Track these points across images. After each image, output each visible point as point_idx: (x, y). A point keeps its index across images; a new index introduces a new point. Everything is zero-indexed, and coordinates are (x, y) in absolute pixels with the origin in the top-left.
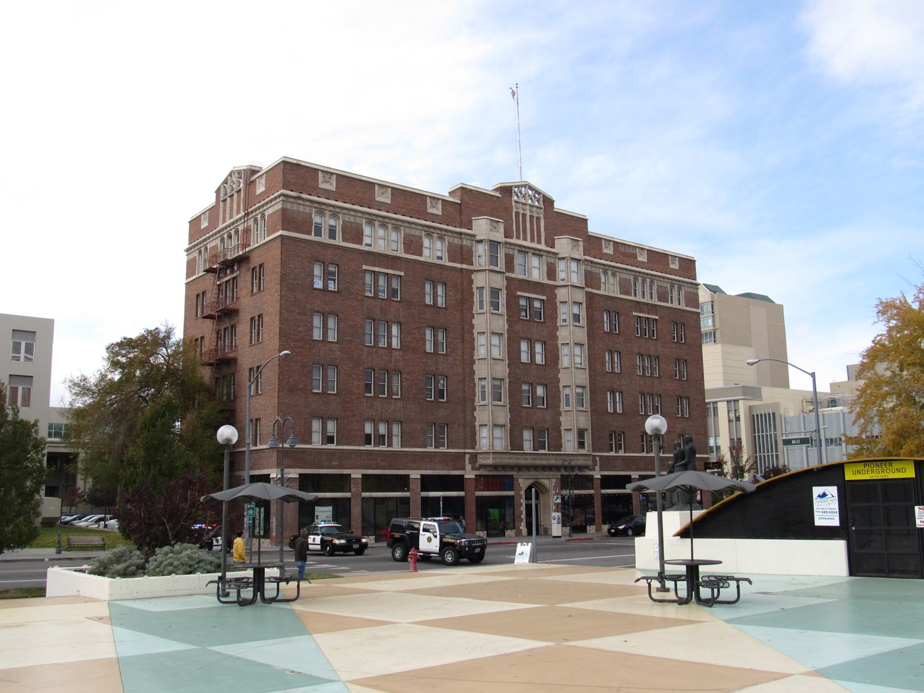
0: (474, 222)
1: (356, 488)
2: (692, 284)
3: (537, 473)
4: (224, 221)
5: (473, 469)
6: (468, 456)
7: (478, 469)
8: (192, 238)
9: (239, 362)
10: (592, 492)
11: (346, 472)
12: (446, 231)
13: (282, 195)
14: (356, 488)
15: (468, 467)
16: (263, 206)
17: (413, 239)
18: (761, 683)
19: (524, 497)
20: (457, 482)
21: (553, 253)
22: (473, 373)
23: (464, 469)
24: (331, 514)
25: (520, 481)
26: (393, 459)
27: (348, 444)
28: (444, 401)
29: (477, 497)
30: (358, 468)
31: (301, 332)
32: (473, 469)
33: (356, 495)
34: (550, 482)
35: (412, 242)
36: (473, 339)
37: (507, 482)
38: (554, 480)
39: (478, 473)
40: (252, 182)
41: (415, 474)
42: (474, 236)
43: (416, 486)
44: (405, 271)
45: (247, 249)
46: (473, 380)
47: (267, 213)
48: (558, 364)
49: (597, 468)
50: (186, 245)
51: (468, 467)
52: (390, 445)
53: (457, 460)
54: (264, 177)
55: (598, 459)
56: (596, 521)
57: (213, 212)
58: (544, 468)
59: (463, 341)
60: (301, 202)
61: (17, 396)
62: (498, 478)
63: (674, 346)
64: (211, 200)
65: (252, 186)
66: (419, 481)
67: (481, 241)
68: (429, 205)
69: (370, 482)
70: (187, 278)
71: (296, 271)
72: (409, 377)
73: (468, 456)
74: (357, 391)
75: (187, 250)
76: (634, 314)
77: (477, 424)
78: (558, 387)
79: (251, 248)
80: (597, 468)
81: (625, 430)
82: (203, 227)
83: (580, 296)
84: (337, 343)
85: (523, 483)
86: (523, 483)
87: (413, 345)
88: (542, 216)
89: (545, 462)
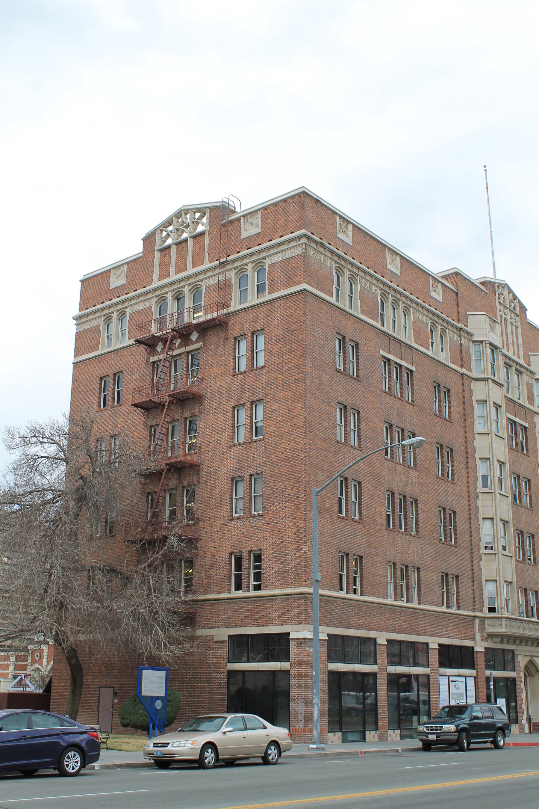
3: (533, 649)
4: (164, 274)
6: (477, 621)
8: (84, 303)
9: (206, 468)
10: (392, 669)
11: (371, 634)
13: (305, 235)
15: (478, 636)
16: (123, 302)
29: (389, 674)
30: (383, 630)
40: (231, 222)
45: (225, 311)
47: (267, 263)
50: (75, 311)
54: (260, 213)
57: (136, 268)
59: (467, 466)
60: (321, 250)
61: (358, 419)
64: (136, 248)
65: (231, 228)
70: (76, 356)
75: (76, 319)
79: (231, 309)
82: (112, 286)
87: (426, 465)
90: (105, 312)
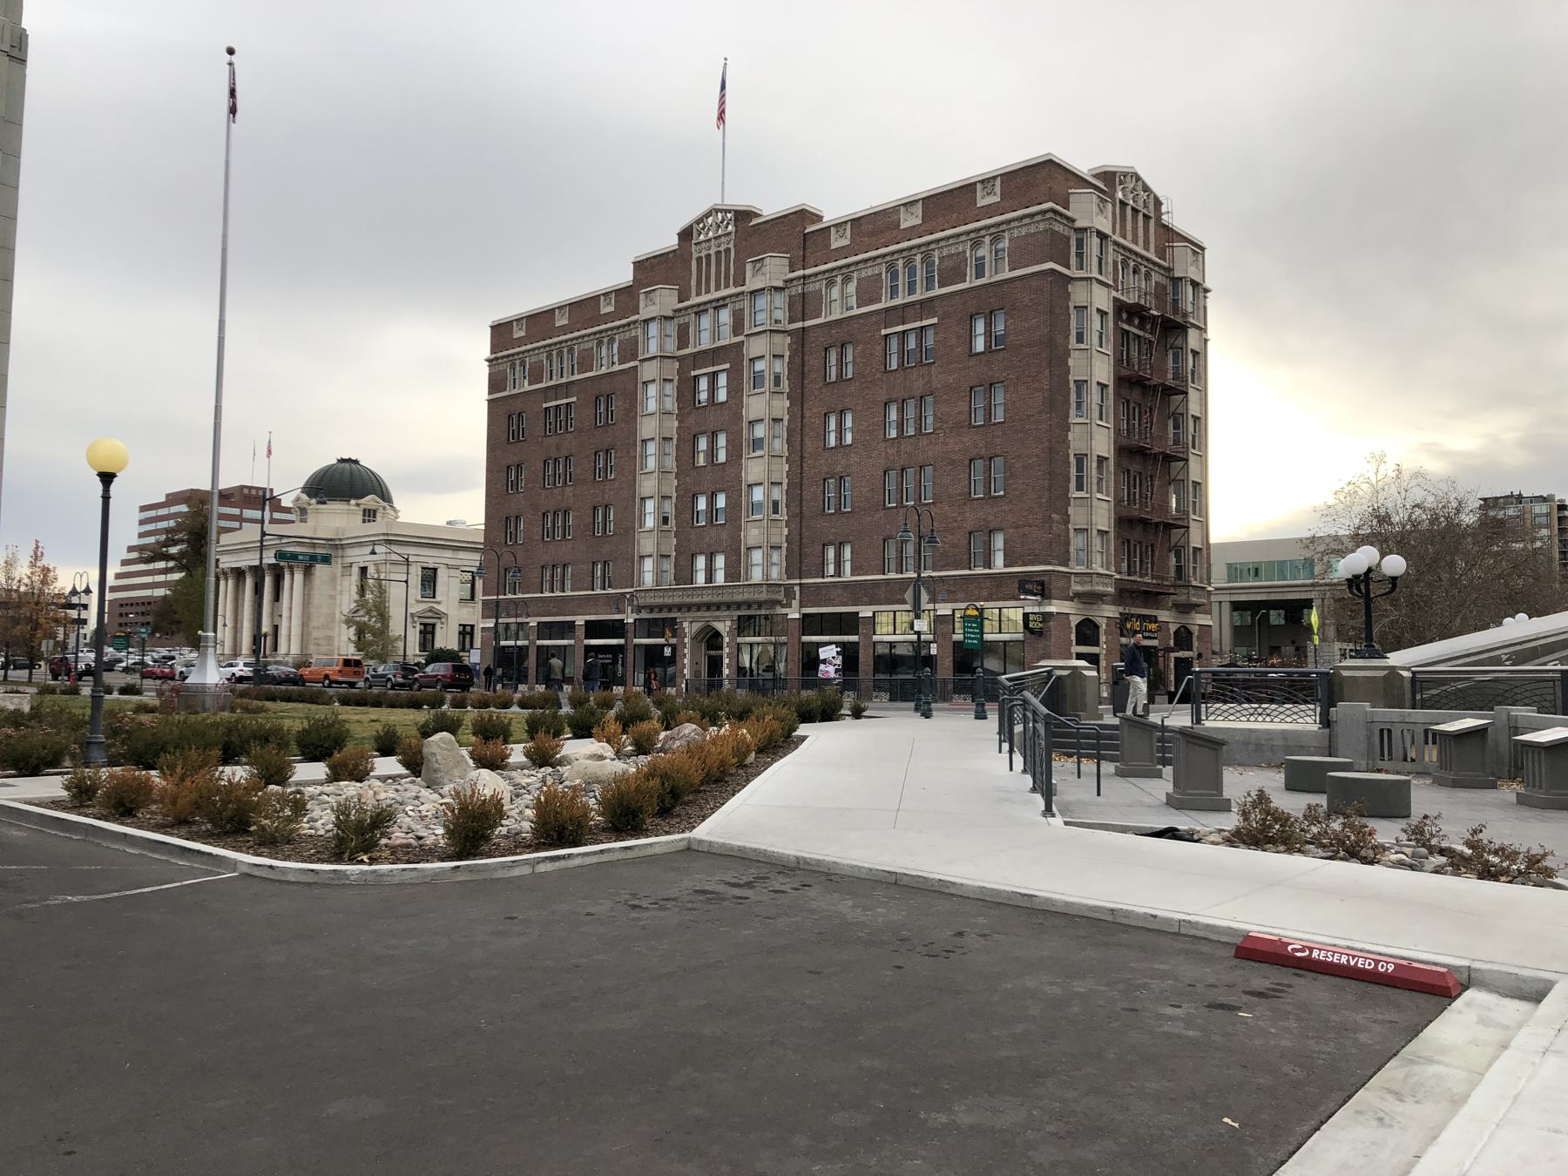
12: (848, 266)
18: (1491, 991)
19: (1102, 631)
20: (616, 629)
21: (1067, 218)
25: (685, 625)
37: (671, 625)
38: (728, 623)
42: (1073, 221)
43: (581, 633)
49: (795, 603)
52: (988, 565)
53: (617, 602)
55: (797, 589)
58: (718, 606)
80: (795, 603)
83: (783, 344)
85: (689, 627)
86: (689, 627)
89: (697, 600)
90: (993, 230)
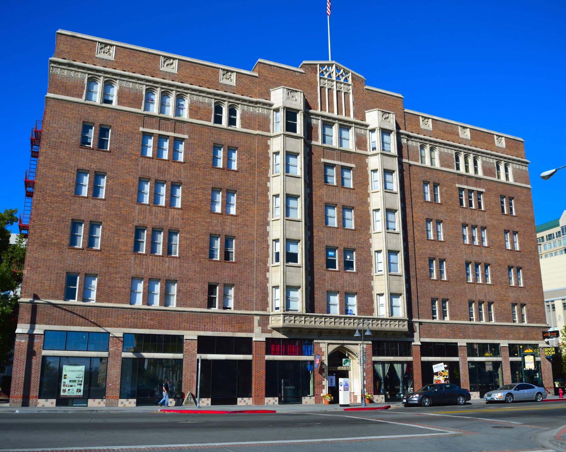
0: (272, 93)
1: (463, 353)
2: (265, 104)
5: (263, 331)
6: (256, 319)
7: (270, 332)
14: (463, 353)
17: (201, 105)
22: (266, 234)
23: (252, 331)
24: (82, 374)
26: (163, 318)
27: (109, 301)
28: (227, 260)
31: (61, 188)
32: (263, 331)
33: (464, 360)
34: (358, 348)
35: (199, 108)
36: (268, 202)
39: (269, 336)
41: (191, 335)
44: (188, 133)
46: (267, 241)
48: (369, 229)
51: (257, 329)
53: (244, 321)
56: (109, 393)
62: (297, 339)
63: (504, 217)
66: (196, 342)
67: (373, 131)
68: (221, 76)
69: (471, 350)
71: (60, 131)
72: (188, 236)
73: (256, 319)
74: (124, 248)
76: (322, 160)
77: (270, 286)
78: (369, 252)
81: (449, 297)
84: (181, 209)
87: (194, 205)
88: (351, 91)
